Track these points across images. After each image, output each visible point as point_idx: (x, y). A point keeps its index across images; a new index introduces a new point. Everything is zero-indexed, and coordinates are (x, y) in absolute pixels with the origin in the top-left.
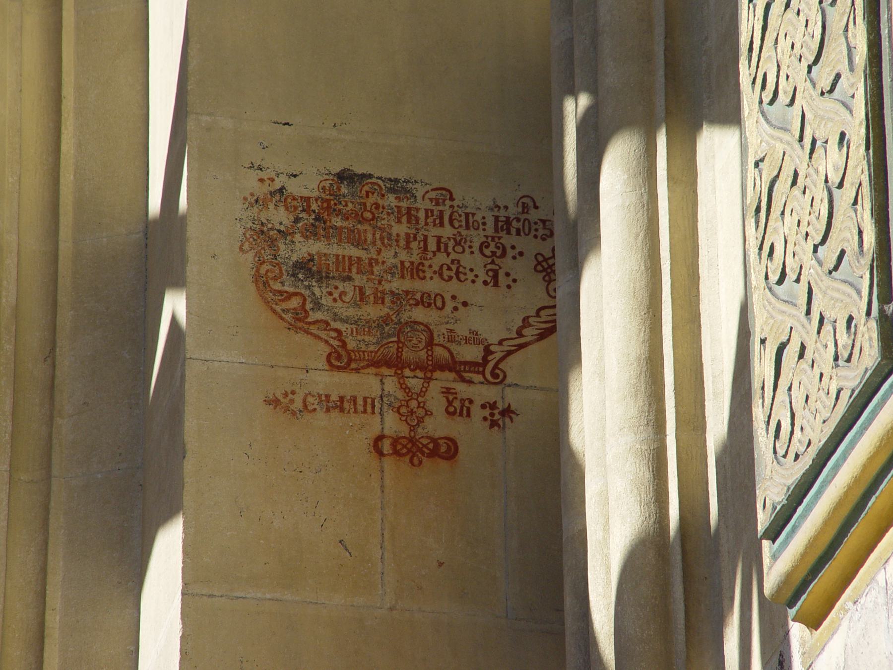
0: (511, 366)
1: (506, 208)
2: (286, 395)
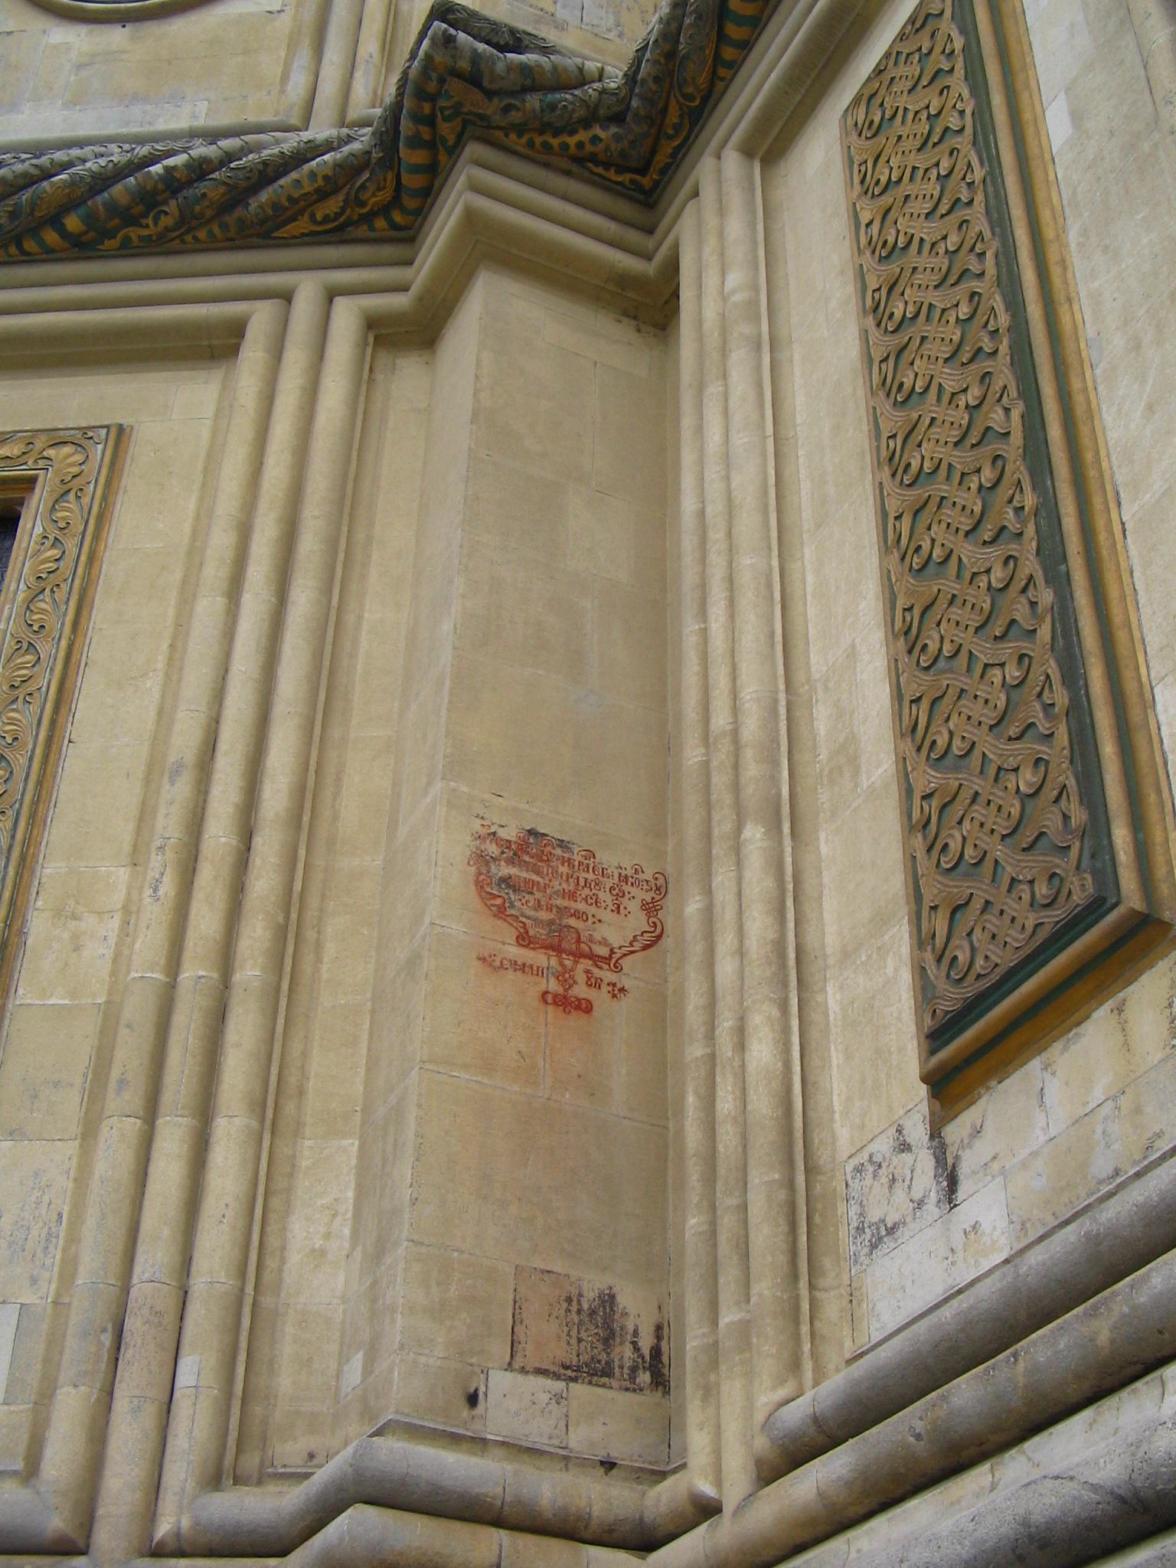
0: (626, 963)
1: (626, 869)
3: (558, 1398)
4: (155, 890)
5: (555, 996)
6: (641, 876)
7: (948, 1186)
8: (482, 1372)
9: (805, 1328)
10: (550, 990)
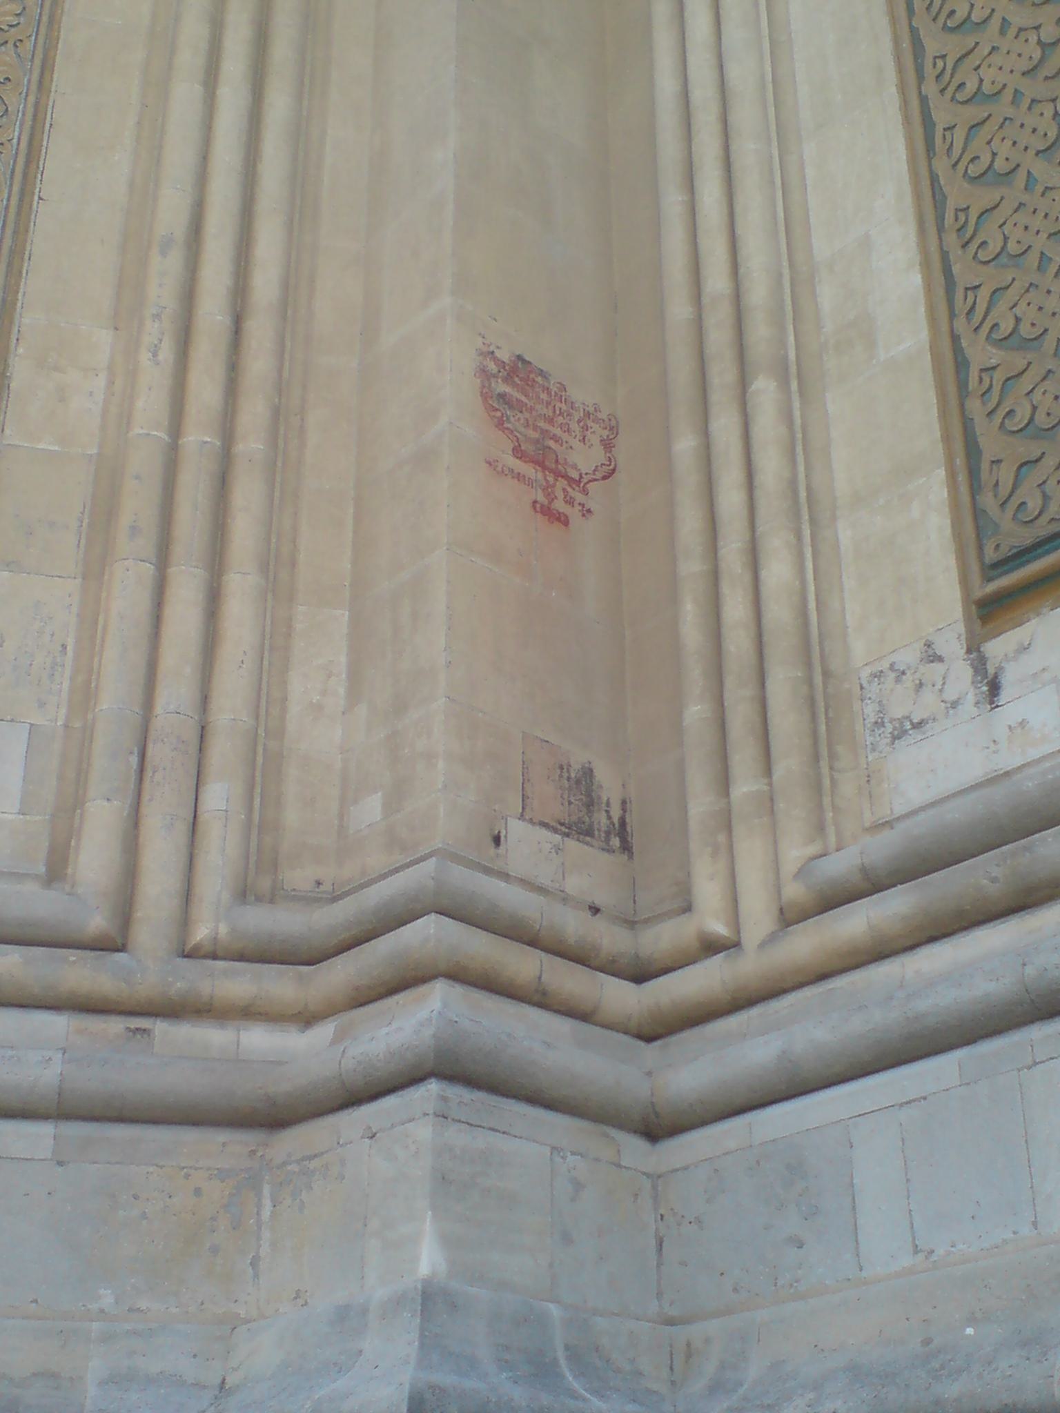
0: (591, 486)
1: (588, 406)
2: (494, 461)
3: (558, 849)
4: (155, 355)
5: (542, 506)
6: (600, 415)
7: (988, 690)
8: (502, 819)
9: (826, 801)
10: (538, 499)
